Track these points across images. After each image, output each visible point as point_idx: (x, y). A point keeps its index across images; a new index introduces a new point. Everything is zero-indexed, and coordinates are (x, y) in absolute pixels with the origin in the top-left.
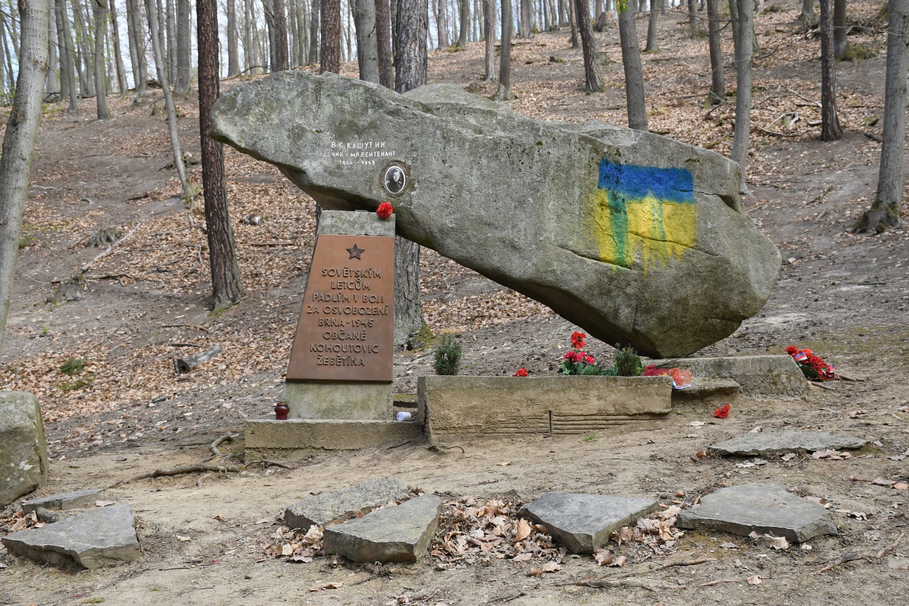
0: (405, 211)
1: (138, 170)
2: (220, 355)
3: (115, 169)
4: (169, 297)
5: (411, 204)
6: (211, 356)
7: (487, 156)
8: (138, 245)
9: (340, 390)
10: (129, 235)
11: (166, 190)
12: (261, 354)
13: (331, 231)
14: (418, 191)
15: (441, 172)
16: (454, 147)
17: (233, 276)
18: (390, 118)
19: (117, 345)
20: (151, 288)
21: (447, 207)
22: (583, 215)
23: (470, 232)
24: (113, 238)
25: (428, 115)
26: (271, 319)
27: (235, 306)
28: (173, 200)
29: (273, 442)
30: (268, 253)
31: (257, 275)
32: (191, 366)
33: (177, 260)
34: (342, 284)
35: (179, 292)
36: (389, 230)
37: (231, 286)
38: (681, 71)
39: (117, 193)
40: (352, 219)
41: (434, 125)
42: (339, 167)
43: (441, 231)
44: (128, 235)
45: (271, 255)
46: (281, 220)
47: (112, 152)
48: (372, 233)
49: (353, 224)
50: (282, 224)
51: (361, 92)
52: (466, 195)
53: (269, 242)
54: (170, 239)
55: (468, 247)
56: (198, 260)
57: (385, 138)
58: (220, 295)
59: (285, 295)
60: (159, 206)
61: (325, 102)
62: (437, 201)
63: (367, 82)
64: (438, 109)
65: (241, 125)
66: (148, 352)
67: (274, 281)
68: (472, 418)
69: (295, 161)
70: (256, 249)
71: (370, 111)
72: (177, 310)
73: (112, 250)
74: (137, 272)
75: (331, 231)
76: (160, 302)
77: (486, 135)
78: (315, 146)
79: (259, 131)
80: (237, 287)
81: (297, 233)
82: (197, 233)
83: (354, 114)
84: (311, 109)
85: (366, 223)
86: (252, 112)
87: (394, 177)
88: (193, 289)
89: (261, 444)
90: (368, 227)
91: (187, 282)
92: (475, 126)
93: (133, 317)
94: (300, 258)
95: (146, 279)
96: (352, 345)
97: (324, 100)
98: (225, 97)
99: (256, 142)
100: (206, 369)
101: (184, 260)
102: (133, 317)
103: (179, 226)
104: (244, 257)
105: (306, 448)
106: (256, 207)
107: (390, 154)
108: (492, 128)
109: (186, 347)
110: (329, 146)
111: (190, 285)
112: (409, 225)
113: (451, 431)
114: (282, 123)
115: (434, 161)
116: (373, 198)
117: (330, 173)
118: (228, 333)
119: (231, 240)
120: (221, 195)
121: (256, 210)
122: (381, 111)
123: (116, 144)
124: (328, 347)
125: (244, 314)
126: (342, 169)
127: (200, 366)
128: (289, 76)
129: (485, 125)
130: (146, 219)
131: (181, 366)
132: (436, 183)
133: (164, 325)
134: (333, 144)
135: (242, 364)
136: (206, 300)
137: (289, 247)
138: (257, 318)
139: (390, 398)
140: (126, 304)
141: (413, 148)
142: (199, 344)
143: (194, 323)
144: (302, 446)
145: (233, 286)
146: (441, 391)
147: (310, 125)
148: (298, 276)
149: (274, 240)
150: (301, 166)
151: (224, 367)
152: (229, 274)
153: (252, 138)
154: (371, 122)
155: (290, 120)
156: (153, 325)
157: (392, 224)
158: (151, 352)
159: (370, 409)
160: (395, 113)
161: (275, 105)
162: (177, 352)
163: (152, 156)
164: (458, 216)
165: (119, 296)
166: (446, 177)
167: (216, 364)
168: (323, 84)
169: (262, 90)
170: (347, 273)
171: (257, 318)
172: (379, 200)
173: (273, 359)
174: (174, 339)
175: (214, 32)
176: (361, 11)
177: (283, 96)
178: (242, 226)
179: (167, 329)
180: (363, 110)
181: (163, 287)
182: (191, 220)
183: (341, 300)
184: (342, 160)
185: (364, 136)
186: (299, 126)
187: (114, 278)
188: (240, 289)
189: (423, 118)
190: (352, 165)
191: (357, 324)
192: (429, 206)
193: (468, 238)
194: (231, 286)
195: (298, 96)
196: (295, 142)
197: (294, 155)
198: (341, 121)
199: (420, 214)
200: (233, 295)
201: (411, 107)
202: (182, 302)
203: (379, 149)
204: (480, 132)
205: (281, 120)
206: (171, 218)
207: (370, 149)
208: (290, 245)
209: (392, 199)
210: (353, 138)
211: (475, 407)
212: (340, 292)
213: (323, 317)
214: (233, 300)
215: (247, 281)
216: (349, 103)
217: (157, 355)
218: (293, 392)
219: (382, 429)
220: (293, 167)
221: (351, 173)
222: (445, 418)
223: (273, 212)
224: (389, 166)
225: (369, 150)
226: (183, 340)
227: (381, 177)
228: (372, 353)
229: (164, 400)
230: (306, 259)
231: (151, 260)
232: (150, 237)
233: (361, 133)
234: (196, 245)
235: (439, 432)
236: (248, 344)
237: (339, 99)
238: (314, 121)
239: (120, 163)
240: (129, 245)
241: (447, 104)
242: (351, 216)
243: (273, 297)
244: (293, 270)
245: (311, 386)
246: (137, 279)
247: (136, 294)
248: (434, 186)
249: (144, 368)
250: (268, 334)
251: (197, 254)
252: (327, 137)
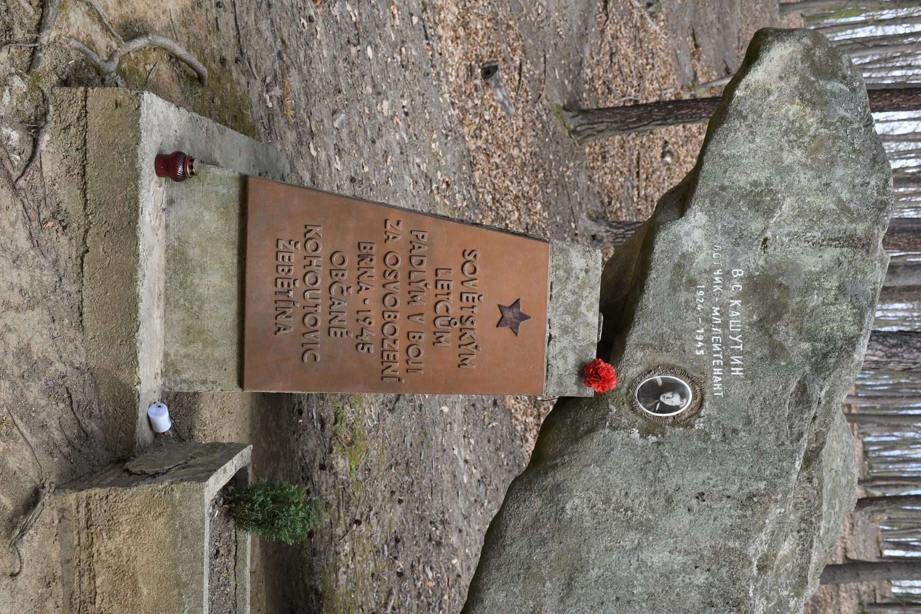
0: (598, 415)
1: (725, 40)
2: (504, 113)
3: (726, 17)
4: (581, 63)
5: (614, 429)
6: (502, 103)
7: (712, 585)
8: (642, 35)
9: (226, 285)
10: (652, 26)
11: (702, 66)
12: (504, 160)
13: (557, 267)
14: (640, 442)
15: (678, 489)
16: (731, 516)
17: (601, 131)
18: (793, 387)
19: (525, 4)
20: (592, 45)
21: (607, 501)
23: (554, 546)
24: (651, 9)
25: (798, 465)
26: (550, 172)
27: (567, 134)
28: (692, 74)
29: (99, 146)
30: (630, 171)
31: (604, 157)
32: (489, 81)
33: (624, 74)
34: (446, 290)
35: (587, 75)
36: (560, 384)
37: (590, 129)
38: (825, 601)
39: (700, 18)
40: (583, 309)
41: (777, 476)
42: (692, 283)
43: (558, 487)
44: (654, 26)
45: (627, 174)
46: (667, 184)
47: (745, 15)
48: (553, 349)
49: (573, 311)
50: (662, 186)
51: (847, 328)
52: (631, 539)
53: (642, 171)
54: (648, 67)
55: (524, 542)
56: (624, 96)
57: (751, 375)
58: (580, 117)
59: (579, 188)
60: (685, 59)
61: (826, 256)
62: (618, 481)
63: (866, 342)
64: (810, 480)
65: (780, 90)
66: (513, 37)
67: (597, 176)
68: (113, 583)
69: (705, 196)
70: (634, 157)
71: (806, 346)
72: (565, 71)
73: (637, 8)
74: (611, 32)
75: (557, 267)
76: (575, 53)
77: (757, 580)
78: (736, 235)
79: (769, 125)
80: (589, 135)
81: (652, 201)
82: (654, 96)
83: (800, 312)
84: (812, 228)
85: (575, 338)
86: (808, 110)
87: (669, 395)
88: (590, 90)
89: (95, 121)
90: (565, 341)
91: (598, 84)
92: (775, 555)
93: (558, 25)
94: (623, 204)
95: (603, 41)
96: (319, 309)
97: (830, 254)
98: (840, 58)
99: (745, 118)
100: (485, 97)
101: (624, 81)
102: (558, 25)
103: (663, 78)
104: (626, 145)
105: (87, 216)
106: (682, 158)
107: (718, 387)
108: (771, 589)
109: (517, 77)
110: (734, 263)
111: (594, 87)
112: (572, 423)
113: (83, 536)
114: (784, 170)
115: (702, 476)
116: (628, 350)
117: (679, 265)
118: (534, 124)
119: (642, 128)
120: (692, 117)
121: (679, 158)
122: (807, 368)
123: (753, 20)
124: (315, 262)
125: (557, 143)
126: (687, 290)
127: (490, 91)
128: (881, 184)
129: (778, 576)
130: (672, 44)
131: (490, 69)
132: (657, 480)
133: (548, 56)
134: (738, 273)
135: (490, 137)
136: (576, 102)
137: (636, 193)
138: (551, 157)
139: (210, 386)
140: (574, 18)
141: (729, 434)
142: (521, 92)
143: (547, 88)
144: (91, 206)
145: (590, 132)
146: (172, 517)
147: (779, 225)
148: (602, 202)
149: (644, 176)
150: (695, 207)
151: (487, 118)
152: (603, 126)
153: (755, 112)
154: (783, 348)
155: (789, 187)
156: (548, 44)
157: (572, 389)
158: (513, 39)
159: (186, 345)
160: (803, 396)
161: (821, 156)
162: (512, 68)
163: (740, 54)
164: (588, 523)
165: (584, 11)
166: (669, 500)
167: (492, 109)
168: (863, 252)
169: (852, 130)
170: (468, 299)
171: (551, 157)
172: (623, 363)
173: (494, 172)
174: (528, 66)
175: (883, 108)
176: (898, 271)
177: (839, 172)
178: (661, 143)
179: (542, 60)
180: (808, 331)
181: (593, 58)
182: (669, 91)
183: (414, 287)
184: (706, 290)
185: (755, 334)
186: (777, 204)
187: (605, 7)
188: (587, 139)
189: (792, 455)
190: (694, 309)
191: (361, 316)
192: (610, 464)
193: (543, 542)
194: (590, 129)
195: (840, 201)
196: (744, 197)
197: (717, 194)
198: (787, 288)
199: (593, 445)
200: (580, 132)
201: (816, 427)
202: (574, 77)
203: (727, 364)
204: (762, 569)
205: (789, 169)
206: (671, 70)
207: (727, 346)
208: (639, 194)
209: (624, 390)
210: (752, 312)
211: (136, 591)
212: (430, 287)
213: (377, 251)
214: (574, 132)
215: (597, 148)
216: (824, 304)
217: (510, 46)
218: (222, 190)
219: (124, 376)
220: (694, 191)
221: (678, 307)
222: (112, 525)
223: (676, 176)
224: (693, 383)
225: (725, 343)
226: (527, 75)
227: (670, 368)
228: (303, 350)
229: (427, 38)
230: (621, 211)
231: (624, 47)
232: (650, 47)
233: (760, 328)
234: (640, 94)
235: (82, 510)
236: (518, 146)
237: (832, 283)
238: (788, 235)
239: (733, 22)
240: (642, 25)
241: (821, 498)
242: (589, 308)
243: (577, 174)
244: (609, 197)
245: (234, 226)
246: (602, 31)
247: (586, 29)
248: (650, 475)
249: (493, 31)
250: (530, 169)
251: (630, 95)
252: (754, 259)
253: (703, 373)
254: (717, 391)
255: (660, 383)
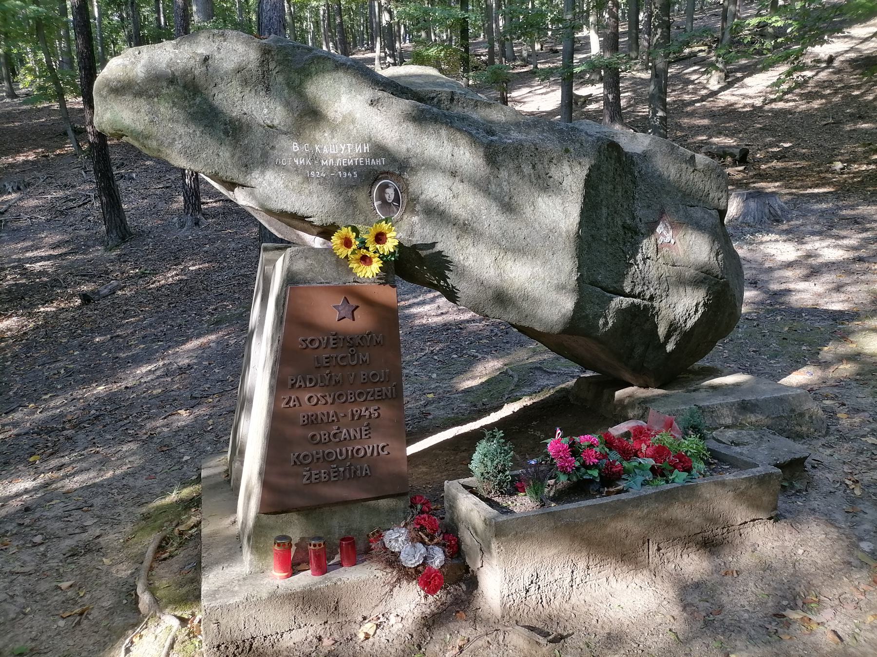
22: (610, 242)
77: (501, 137)
107: (378, 162)
253: (370, 173)
254: (382, 162)
255: (379, 202)
